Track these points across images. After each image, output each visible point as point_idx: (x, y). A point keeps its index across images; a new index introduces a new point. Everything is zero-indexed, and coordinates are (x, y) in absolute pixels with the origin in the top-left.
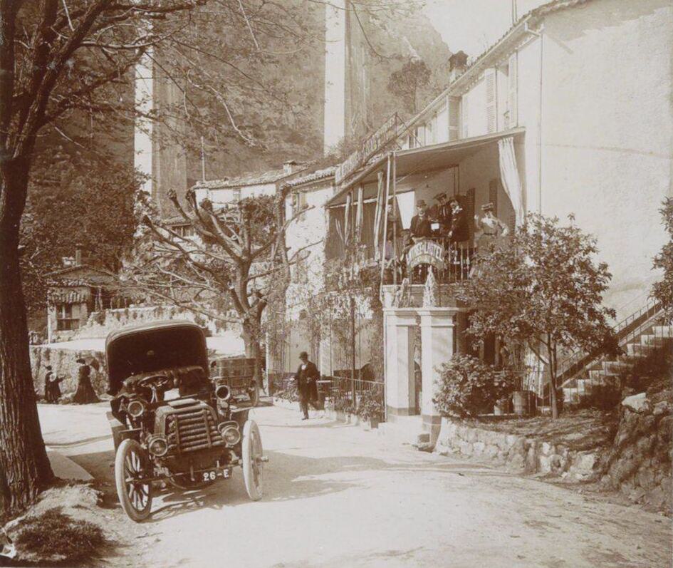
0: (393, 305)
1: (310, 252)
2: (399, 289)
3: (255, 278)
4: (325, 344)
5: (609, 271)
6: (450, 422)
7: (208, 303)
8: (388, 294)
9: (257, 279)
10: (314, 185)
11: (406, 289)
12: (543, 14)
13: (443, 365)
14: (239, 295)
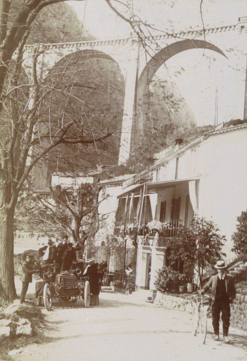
0: (141, 244)
1: (108, 216)
2: (145, 238)
3: (82, 226)
4: (112, 257)
5: (226, 238)
6: (160, 293)
7: (57, 233)
8: (140, 239)
9: (83, 226)
10: (113, 184)
11: (147, 238)
12: (209, 135)
13: (159, 270)
14: (76, 233)
